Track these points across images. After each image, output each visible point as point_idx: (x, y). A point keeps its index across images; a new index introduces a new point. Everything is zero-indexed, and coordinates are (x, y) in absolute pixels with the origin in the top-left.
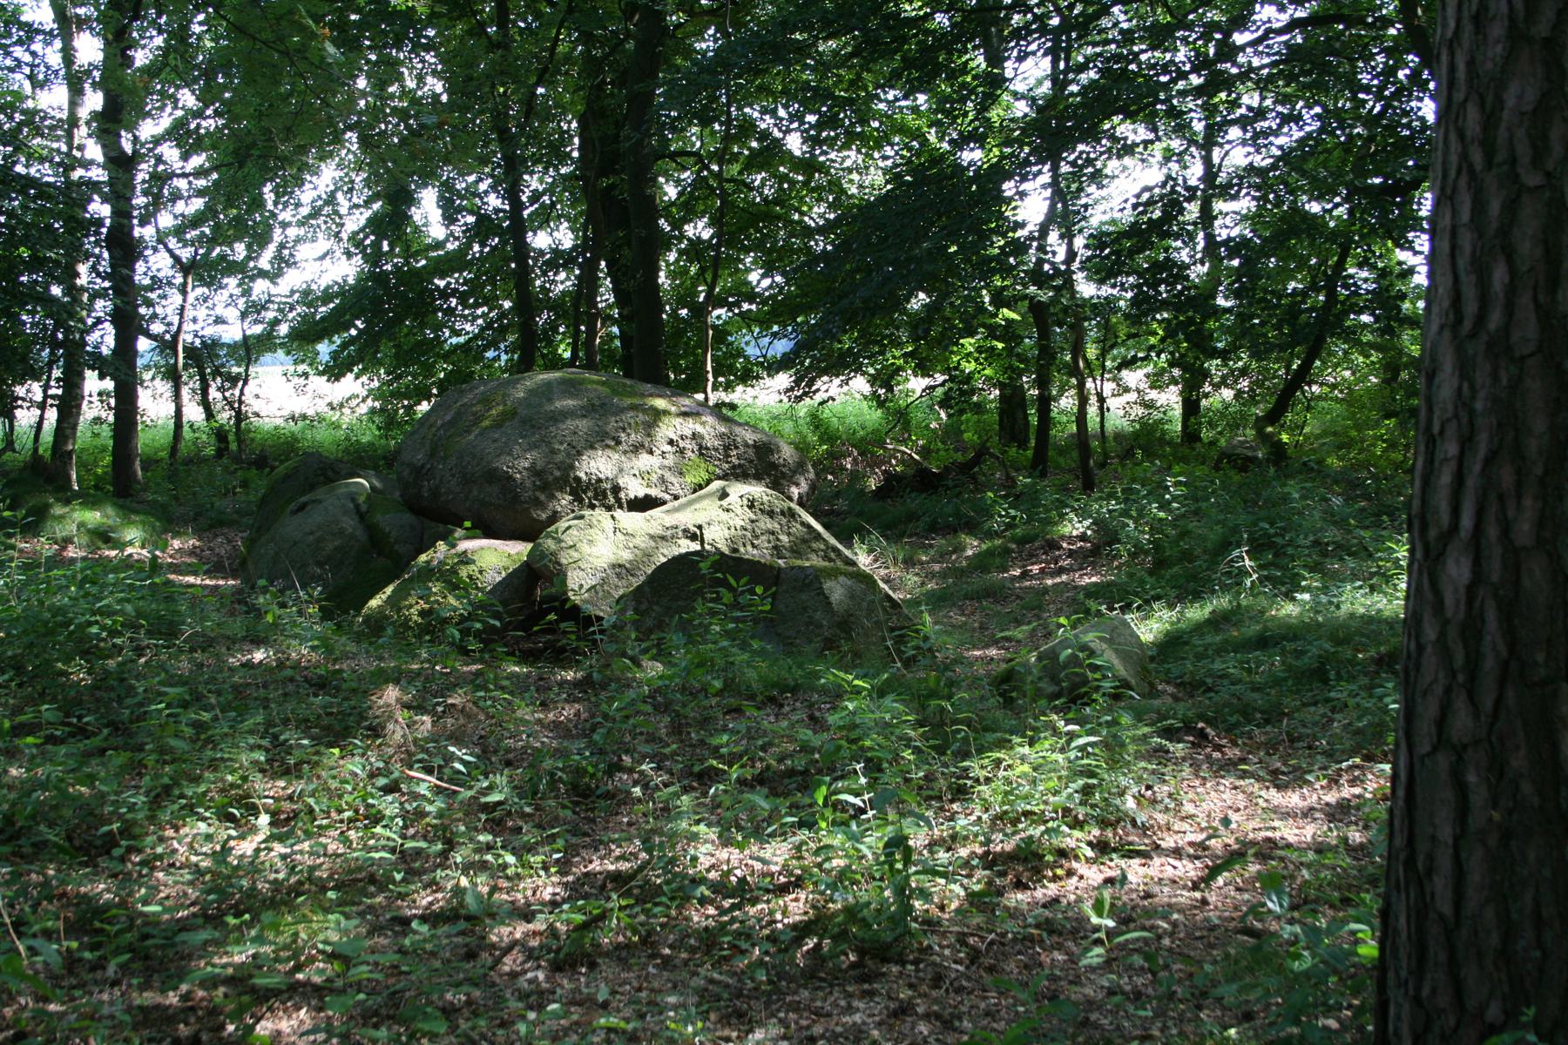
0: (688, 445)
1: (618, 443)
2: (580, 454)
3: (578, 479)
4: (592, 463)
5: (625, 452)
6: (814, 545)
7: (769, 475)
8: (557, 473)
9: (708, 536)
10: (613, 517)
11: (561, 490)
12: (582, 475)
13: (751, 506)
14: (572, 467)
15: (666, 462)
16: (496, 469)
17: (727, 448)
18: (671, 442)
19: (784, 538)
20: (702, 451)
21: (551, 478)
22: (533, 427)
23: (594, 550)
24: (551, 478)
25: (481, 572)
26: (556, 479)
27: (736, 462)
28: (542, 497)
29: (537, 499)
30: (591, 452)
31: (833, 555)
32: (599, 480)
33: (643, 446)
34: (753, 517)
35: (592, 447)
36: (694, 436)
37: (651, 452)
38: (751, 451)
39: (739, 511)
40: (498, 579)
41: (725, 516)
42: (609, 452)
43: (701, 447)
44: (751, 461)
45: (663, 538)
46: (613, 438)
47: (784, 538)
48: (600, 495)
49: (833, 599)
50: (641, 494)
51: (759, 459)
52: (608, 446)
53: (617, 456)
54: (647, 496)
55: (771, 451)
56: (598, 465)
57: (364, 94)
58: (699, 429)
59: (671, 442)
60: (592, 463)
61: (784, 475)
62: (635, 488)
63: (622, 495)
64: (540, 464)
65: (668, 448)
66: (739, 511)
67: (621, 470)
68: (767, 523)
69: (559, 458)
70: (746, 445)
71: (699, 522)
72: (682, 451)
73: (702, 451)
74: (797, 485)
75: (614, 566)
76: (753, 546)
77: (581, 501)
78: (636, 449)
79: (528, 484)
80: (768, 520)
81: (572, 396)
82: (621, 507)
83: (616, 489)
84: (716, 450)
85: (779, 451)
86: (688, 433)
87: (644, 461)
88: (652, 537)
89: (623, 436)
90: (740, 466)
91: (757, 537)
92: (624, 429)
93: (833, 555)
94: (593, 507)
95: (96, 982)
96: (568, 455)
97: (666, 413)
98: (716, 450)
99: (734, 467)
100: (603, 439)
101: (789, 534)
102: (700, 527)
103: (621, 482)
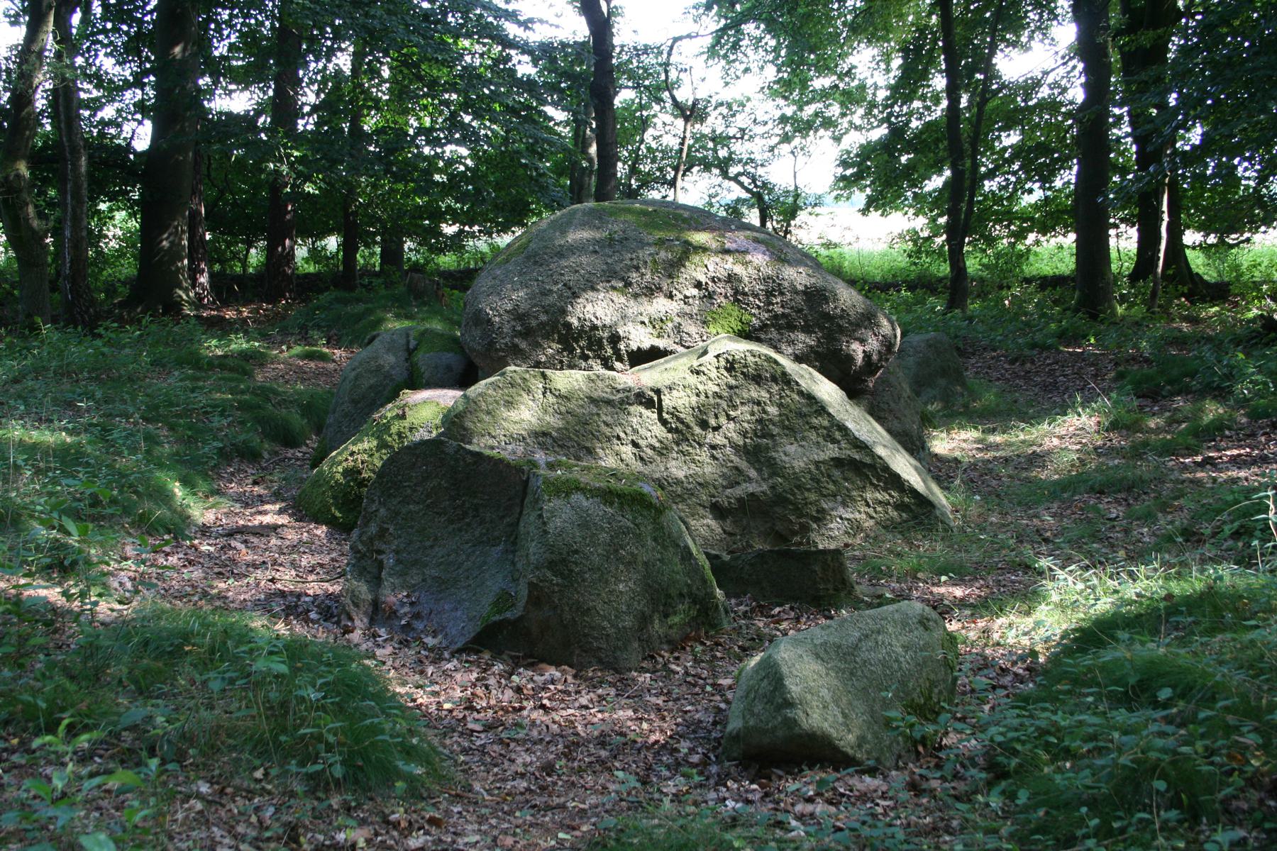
0: (720, 289)
2: (576, 296)
4: (589, 307)
6: (815, 421)
7: (822, 328)
8: (543, 318)
9: (667, 401)
10: (544, 376)
11: (547, 337)
14: (564, 312)
15: (687, 309)
16: (481, 310)
17: (769, 294)
18: (698, 285)
19: (773, 410)
20: (738, 297)
22: (536, 263)
23: (513, 415)
26: (542, 324)
27: (779, 310)
28: (523, 345)
29: (516, 346)
30: (591, 294)
31: (838, 435)
32: (594, 327)
33: (660, 289)
36: (731, 278)
37: (671, 297)
38: (799, 298)
41: (692, 380)
42: (614, 295)
43: (736, 292)
44: (800, 311)
45: (609, 402)
46: (623, 279)
49: (551, 527)
50: (646, 345)
51: (811, 308)
52: (614, 288)
54: (652, 347)
55: (826, 300)
58: (739, 269)
59: (698, 285)
61: (841, 330)
62: (640, 338)
63: (622, 346)
64: (524, 307)
66: (714, 374)
67: (624, 317)
69: (552, 299)
70: (795, 291)
71: (659, 385)
72: (711, 296)
73: (738, 297)
76: (729, 418)
78: (650, 292)
80: (753, 387)
82: (620, 359)
83: (615, 339)
85: (836, 300)
87: (661, 305)
89: (634, 276)
91: (735, 407)
92: (637, 268)
93: (838, 435)
98: (756, 296)
99: (776, 317)
100: (614, 276)
101: (780, 406)
102: (658, 392)
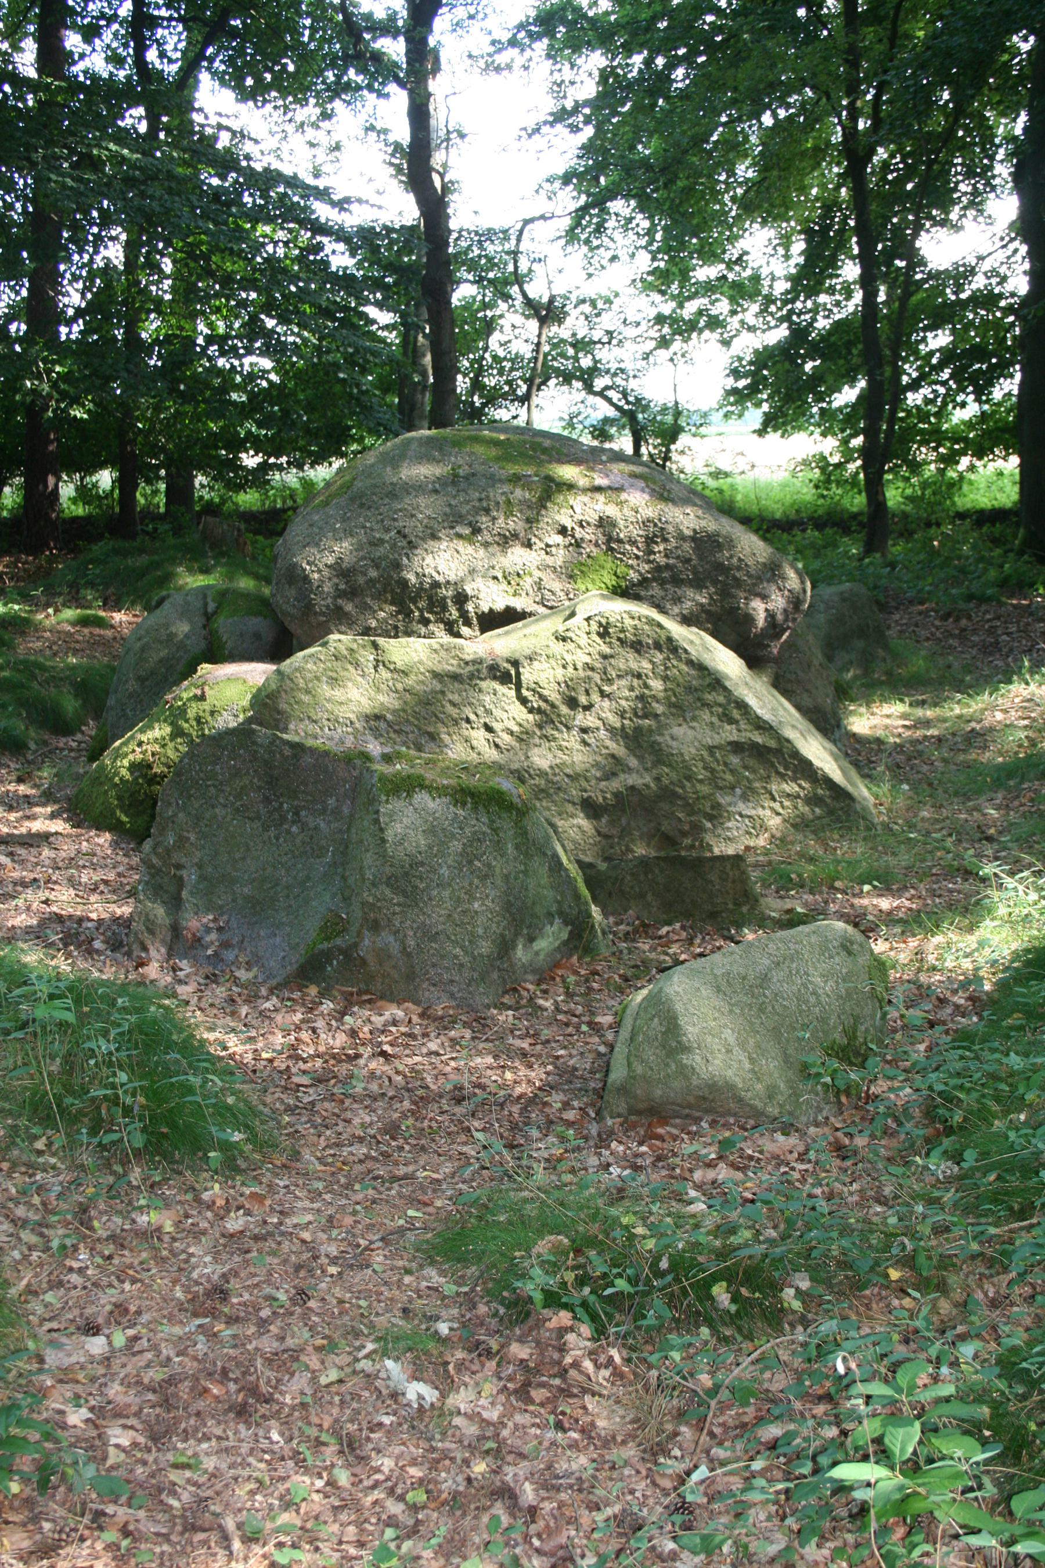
1: (476, 531)
3: (404, 583)
4: (429, 559)
5: (486, 545)
6: (709, 697)
7: (715, 582)
10: (375, 646)
12: (412, 578)
13: (604, 633)
14: (397, 566)
15: (550, 561)
16: (295, 564)
17: (650, 540)
18: (563, 531)
21: (361, 580)
24: (361, 580)
25: (212, 713)
28: (349, 607)
29: (339, 608)
31: (736, 714)
32: (436, 585)
34: (607, 650)
35: (434, 537)
37: (529, 545)
38: (687, 546)
39: (583, 640)
40: (233, 724)
42: (460, 545)
43: (610, 539)
44: (688, 561)
45: (455, 677)
46: (470, 524)
47: (657, 685)
48: (437, 605)
50: (499, 606)
51: (701, 558)
52: (459, 536)
53: (470, 549)
56: (444, 561)
57: (775, 115)
59: (563, 531)
60: (429, 559)
61: (738, 583)
62: (492, 597)
63: (470, 607)
64: (348, 561)
65: (559, 539)
66: (583, 640)
68: (630, 661)
70: (682, 537)
74: (764, 597)
75: (367, 718)
77: (408, 614)
78: (505, 541)
79: (327, 588)
80: (631, 656)
81: (431, 460)
82: (468, 623)
83: (461, 599)
84: (633, 543)
86: (592, 517)
88: (436, 675)
89: (484, 520)
90: (668, 566)
91: (610, 681)
92: (487, 511)
93: (736, 714)
94: (426, 622)
95: (539, 1056)
96: (394, 546)
97: (571, 487)
99: (659, 569)
100: (464, 521)
101: (665, 678)
102: (516, 664)
103: (469, 589)
